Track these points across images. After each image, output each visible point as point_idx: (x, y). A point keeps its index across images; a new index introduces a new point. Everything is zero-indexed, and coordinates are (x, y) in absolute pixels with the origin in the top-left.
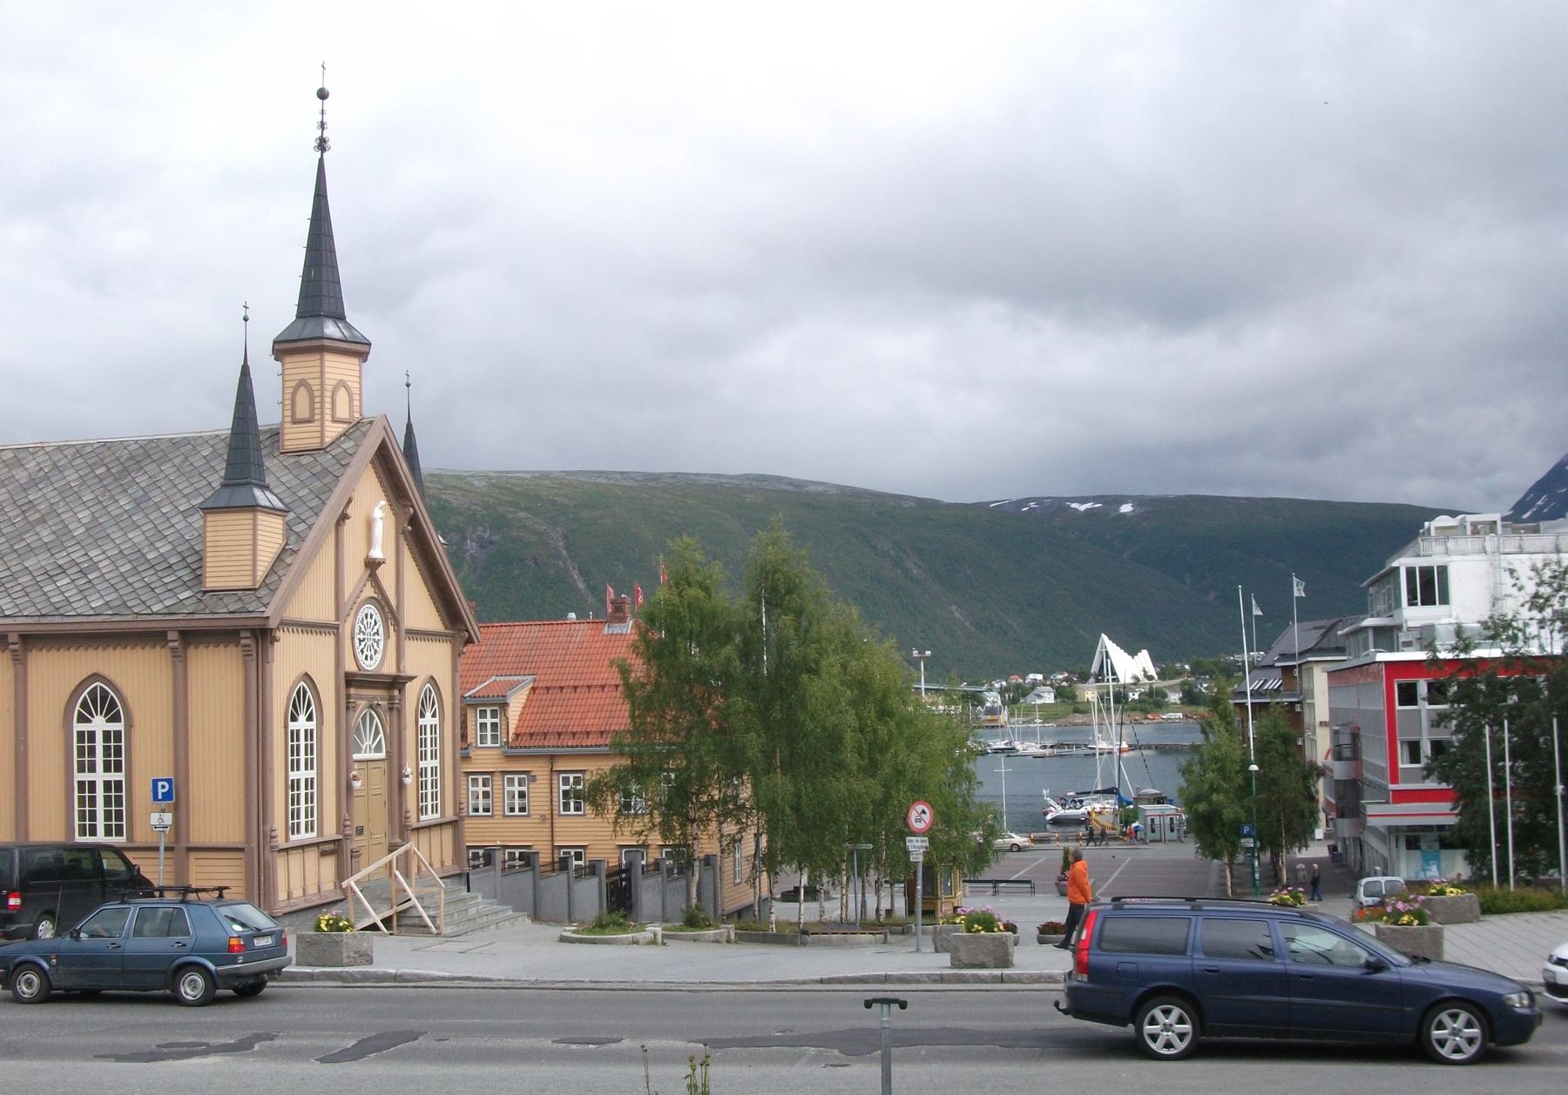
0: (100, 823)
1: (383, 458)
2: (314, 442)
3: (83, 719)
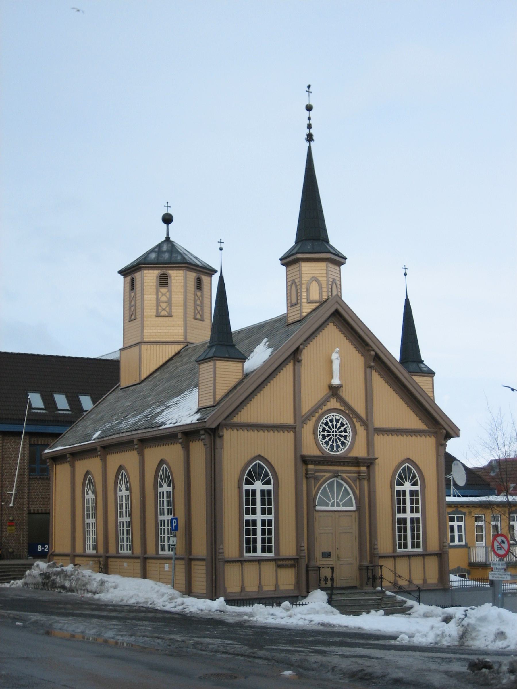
0: (259, 549)
3: (248, 483)
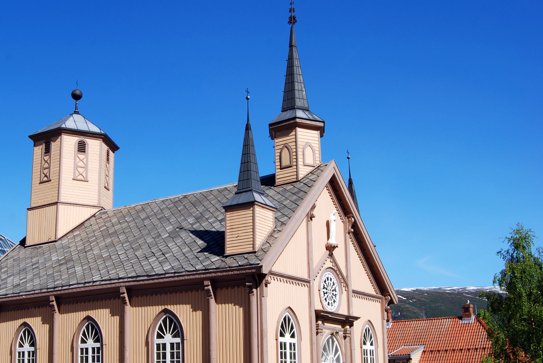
1: (333, 183)
2: (294, 178)
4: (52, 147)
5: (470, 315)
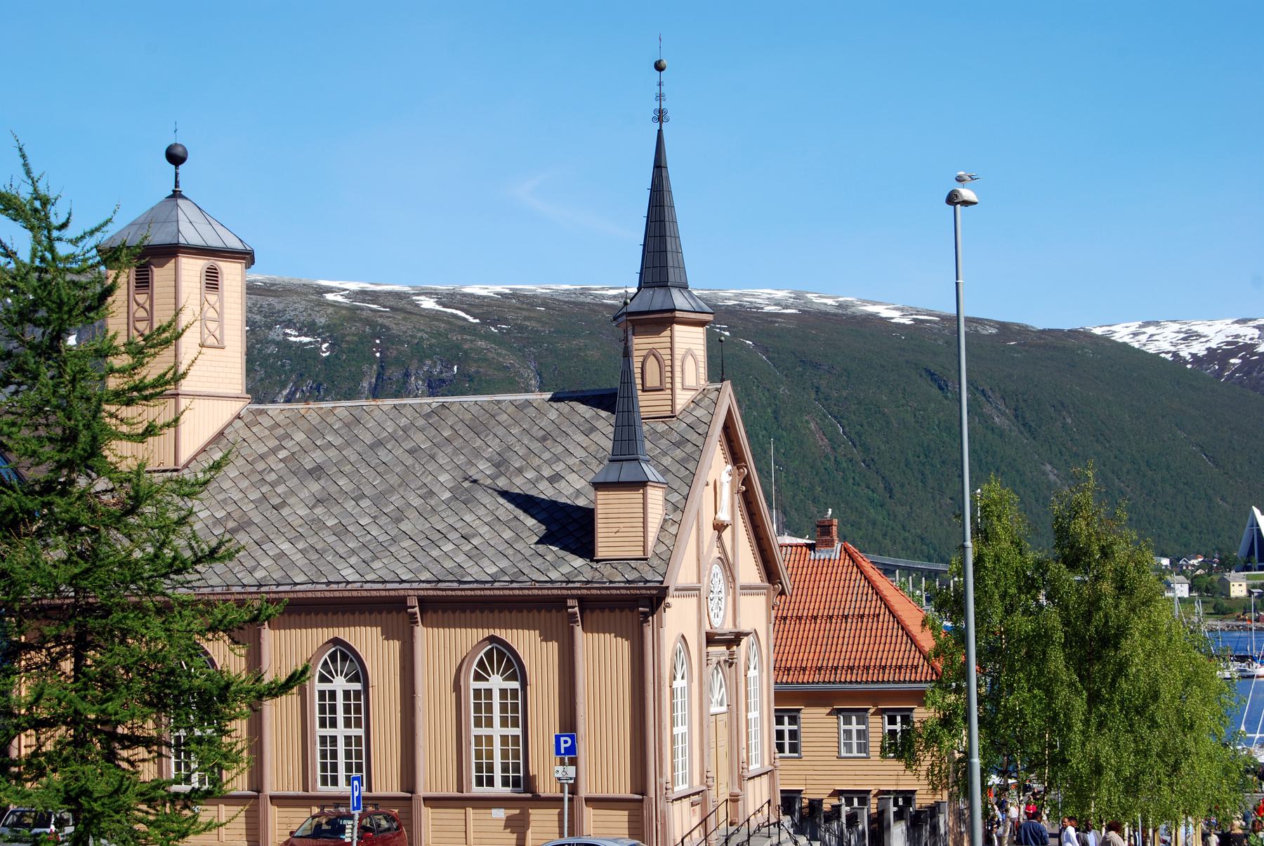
2: (666, 411)
4: (155, 278)
5: (833, 541)
